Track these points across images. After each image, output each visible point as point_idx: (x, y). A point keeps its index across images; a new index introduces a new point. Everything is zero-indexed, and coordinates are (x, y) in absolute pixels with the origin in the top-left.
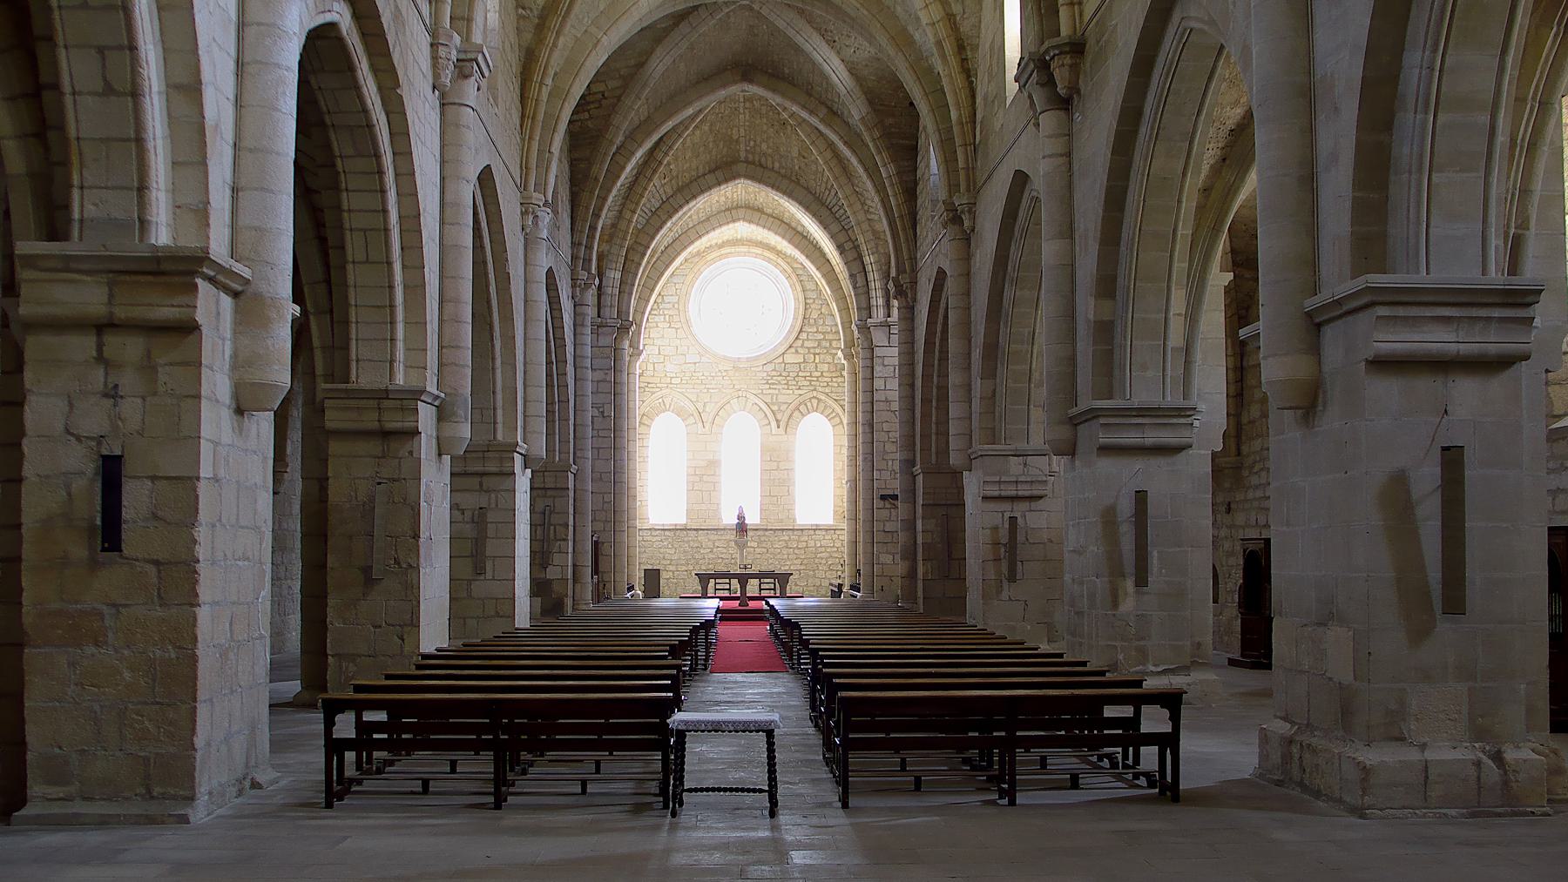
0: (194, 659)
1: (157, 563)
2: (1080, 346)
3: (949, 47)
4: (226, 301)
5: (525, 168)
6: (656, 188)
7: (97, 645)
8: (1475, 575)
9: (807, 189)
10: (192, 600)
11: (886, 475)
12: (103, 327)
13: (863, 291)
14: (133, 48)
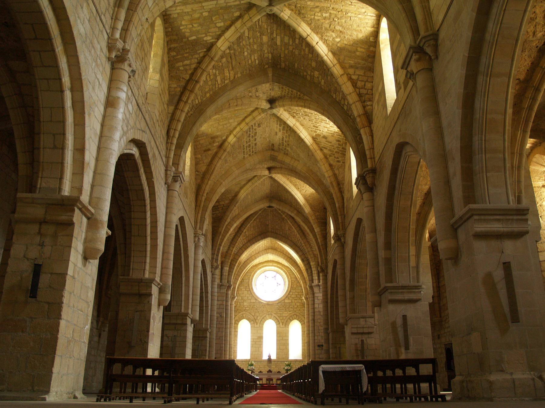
0: (56, 339)
1: (48, 303)
2: (380, 268)
3: (335, 184)
4: (85, 220)
5: (196, 222)
6: (241, 240)
7: (23, 332)
8: (522, 309)
9: (291, 241)
10: (59, 317)
11: (320, 337)
12: (43, 222)
13: (311, 274)
14: (64, 134)
